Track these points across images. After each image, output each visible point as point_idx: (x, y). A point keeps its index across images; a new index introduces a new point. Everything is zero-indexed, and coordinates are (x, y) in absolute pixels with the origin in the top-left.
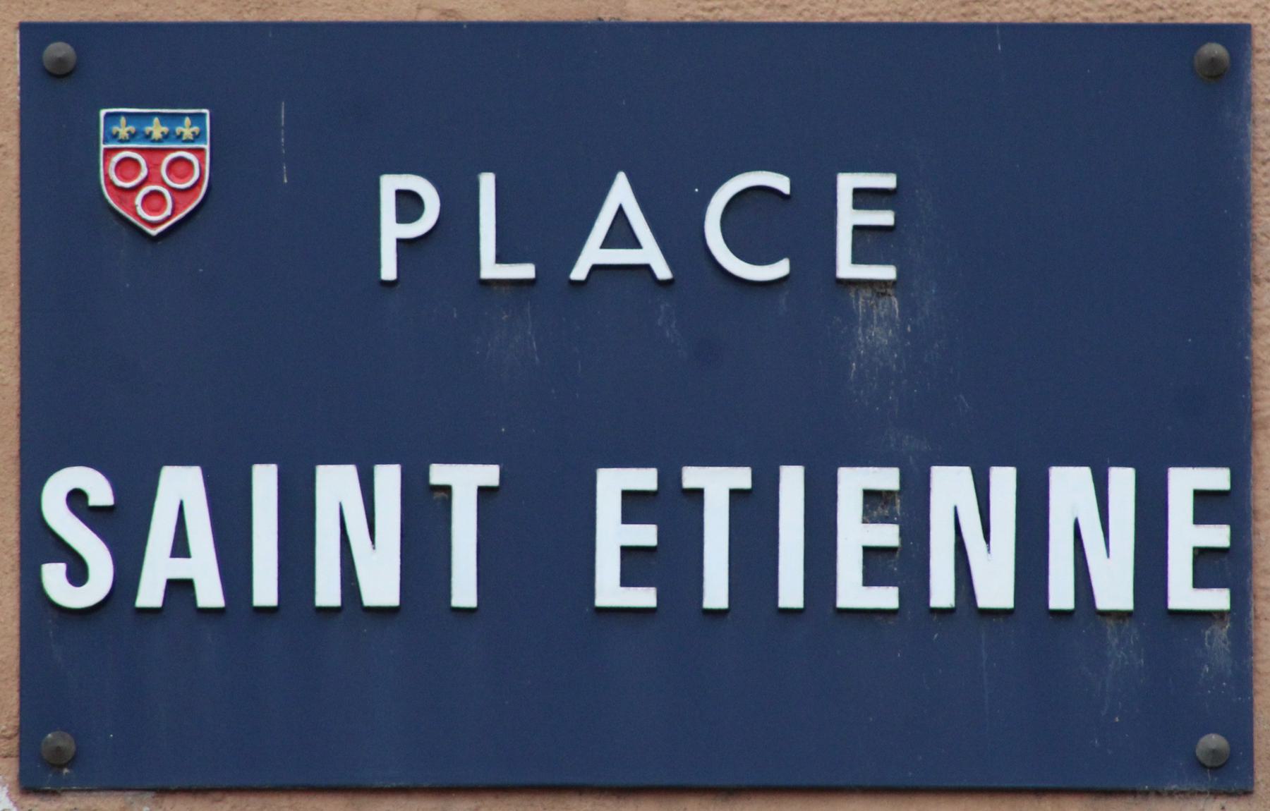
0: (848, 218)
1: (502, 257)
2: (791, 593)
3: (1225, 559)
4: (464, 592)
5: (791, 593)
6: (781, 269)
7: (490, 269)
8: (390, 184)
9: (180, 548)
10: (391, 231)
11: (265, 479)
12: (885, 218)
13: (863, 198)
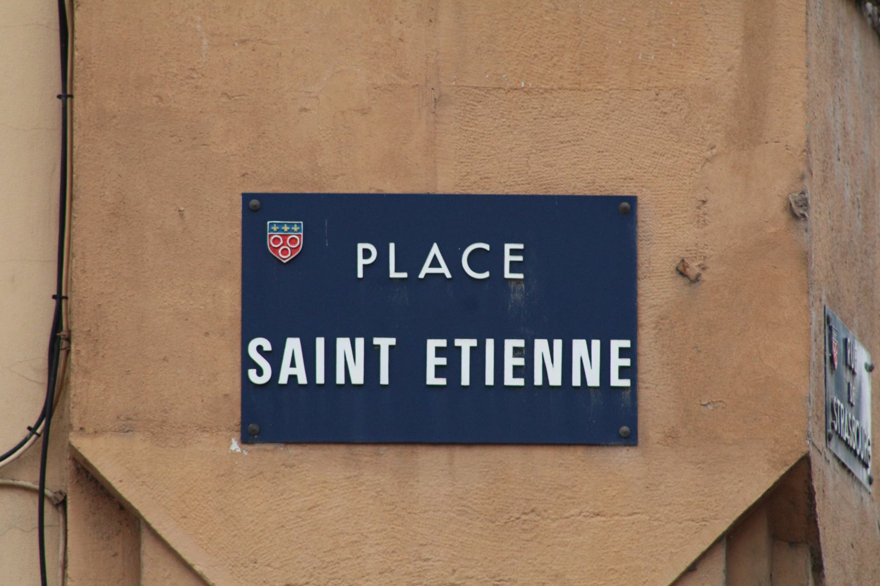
0: (508, 258)
1: (397, 270)
2: (490, 380)
4: (384, 379)
5: (490, 380)
6: (486, 275)
7: (393, 274)
8: (361, 247)
9: (293, 364)
10: (361, 262)
11: (320, 343)
12: (520, 258)
13: (513, 252)
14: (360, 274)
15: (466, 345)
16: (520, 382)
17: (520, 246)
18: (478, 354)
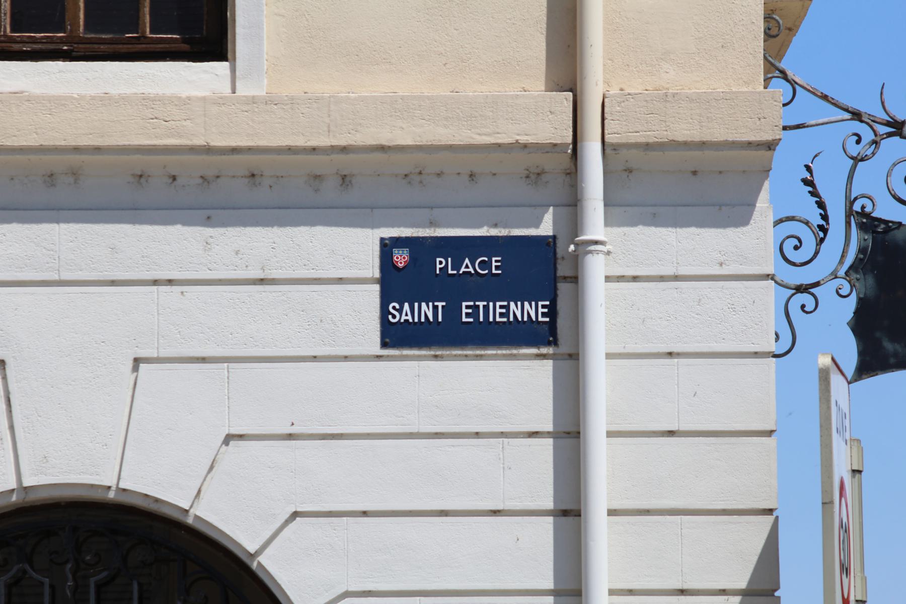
0: (494, 264)
1: (452, 270)
2: (491, 319)
4: (440, 319)
5: (491, 319)
6: (486, 272)
7: (450, 272)
8: (438, 260)
9: (407, 315)
10: (438, 266)
11: (416, 305)
13: (496, 261)
14: (438, 272)
15: (481, 304)
17: (499, 259)
18: (486, 308)
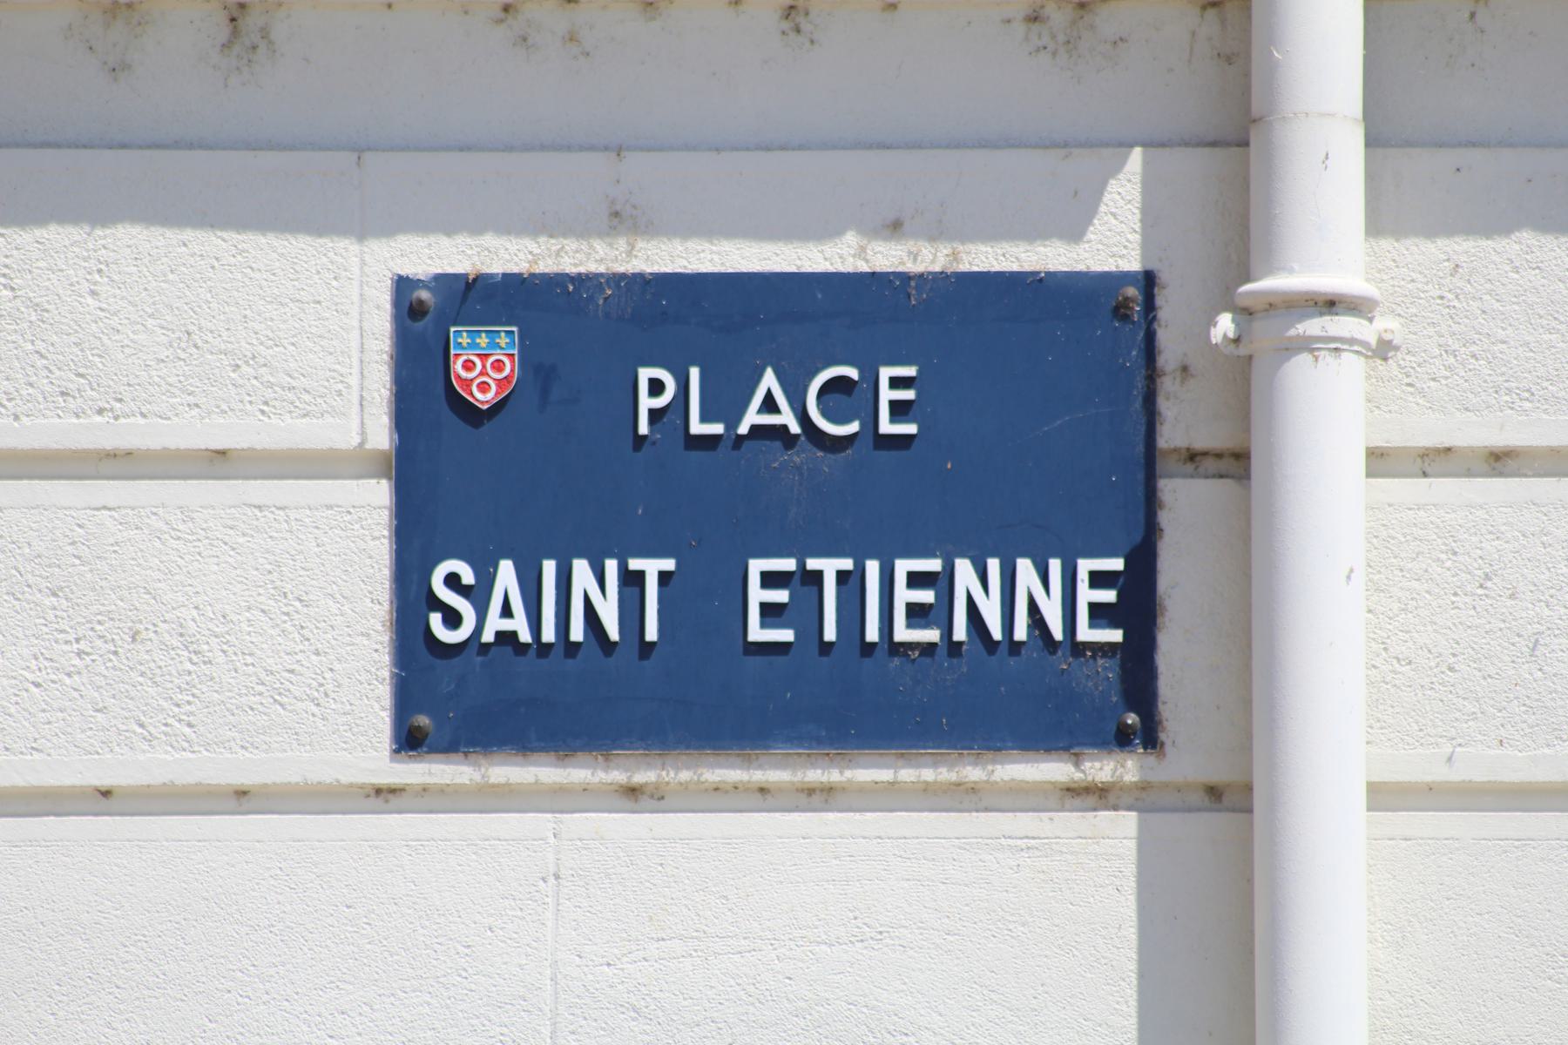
1: (705, 418)
3: (779, 660)
4: (651, 634)
5: (872, 634)
6: (854, 427)
7: (697, 427)
8: (645, 374)
9: (507, 611)
10: (646, 403)
11: (549, 568)
12: (908, 395)
13: (896, 383)
15: (829, 567)
16: (635, 564)
17: (910, 371)
18: (850, 582)
